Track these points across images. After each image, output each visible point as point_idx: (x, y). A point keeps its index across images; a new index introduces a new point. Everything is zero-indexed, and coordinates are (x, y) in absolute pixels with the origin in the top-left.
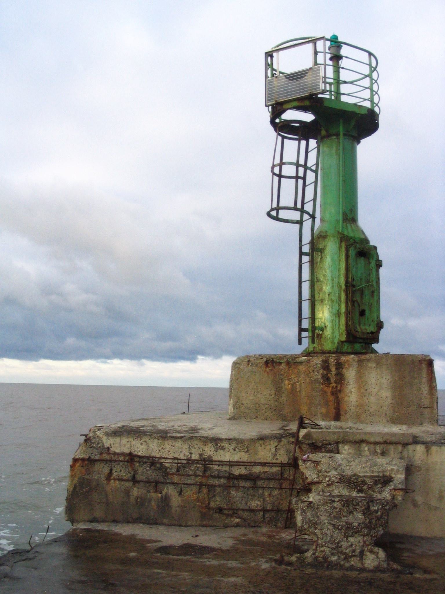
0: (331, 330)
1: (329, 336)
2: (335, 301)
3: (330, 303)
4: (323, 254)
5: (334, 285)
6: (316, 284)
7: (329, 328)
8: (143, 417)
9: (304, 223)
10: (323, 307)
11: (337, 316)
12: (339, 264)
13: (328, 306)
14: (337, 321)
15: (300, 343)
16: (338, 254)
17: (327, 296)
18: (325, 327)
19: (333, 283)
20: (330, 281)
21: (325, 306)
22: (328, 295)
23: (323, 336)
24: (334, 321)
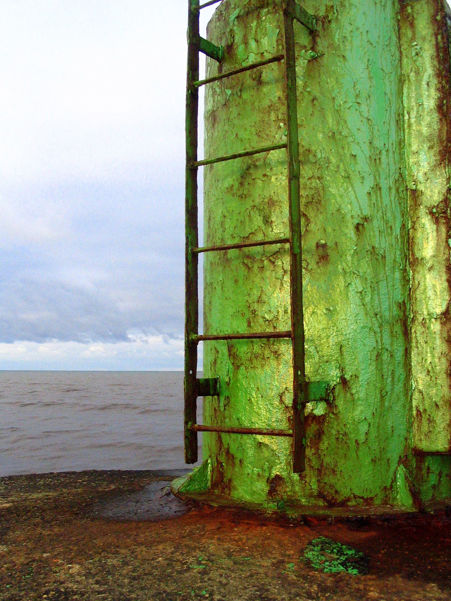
0: (374, 398)
1: (364, 428)
2: (389, 261)
3: (365, 267)
4: (322, 44)
5: (384, 184)
6: (306, 172)
7: (360, 390)
8: (68, 393)
9: (201, 11)
10: (331, 287)
11: (398, 329)
12: (400, 93)
13: (357, 285)
14: (399, 355)
15: (192, 455)
16: (394, 49)
17: (351, 232)
18: (344, 382)
19: (376, 174)
20: (363, 165)
21: (341, 282)
22: (357, 227)
23: (333, 429)
24: (385, 356)
